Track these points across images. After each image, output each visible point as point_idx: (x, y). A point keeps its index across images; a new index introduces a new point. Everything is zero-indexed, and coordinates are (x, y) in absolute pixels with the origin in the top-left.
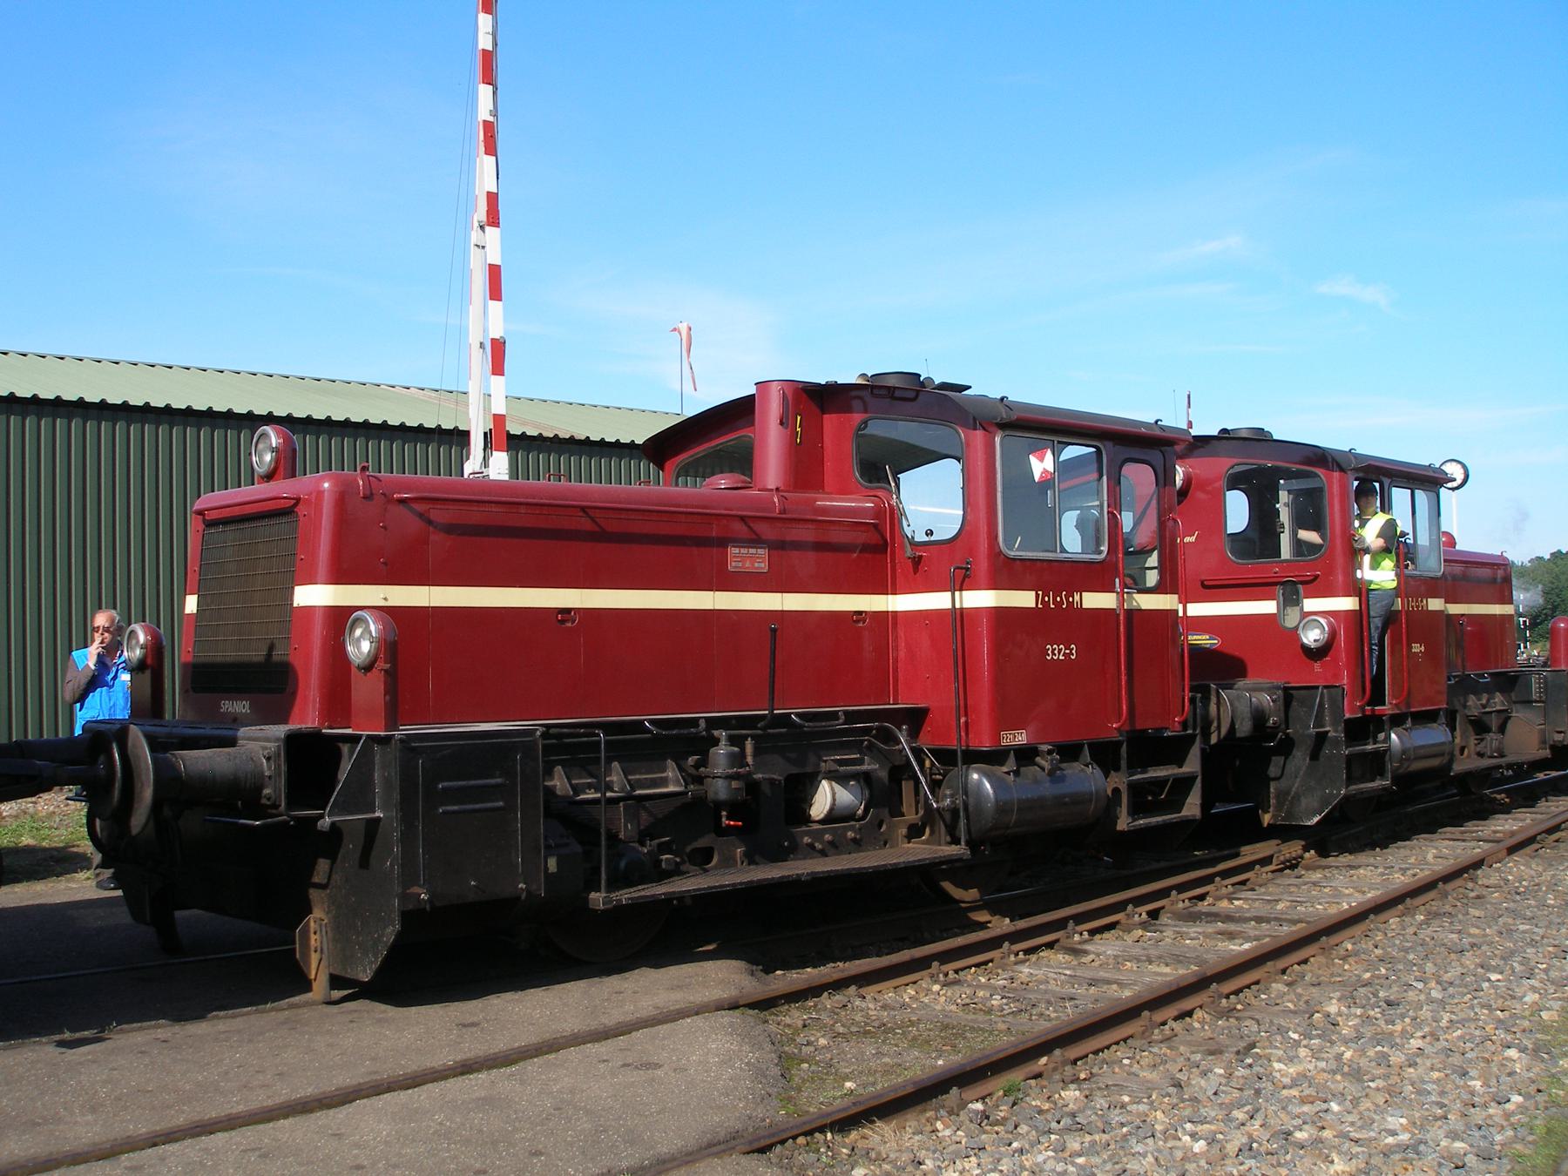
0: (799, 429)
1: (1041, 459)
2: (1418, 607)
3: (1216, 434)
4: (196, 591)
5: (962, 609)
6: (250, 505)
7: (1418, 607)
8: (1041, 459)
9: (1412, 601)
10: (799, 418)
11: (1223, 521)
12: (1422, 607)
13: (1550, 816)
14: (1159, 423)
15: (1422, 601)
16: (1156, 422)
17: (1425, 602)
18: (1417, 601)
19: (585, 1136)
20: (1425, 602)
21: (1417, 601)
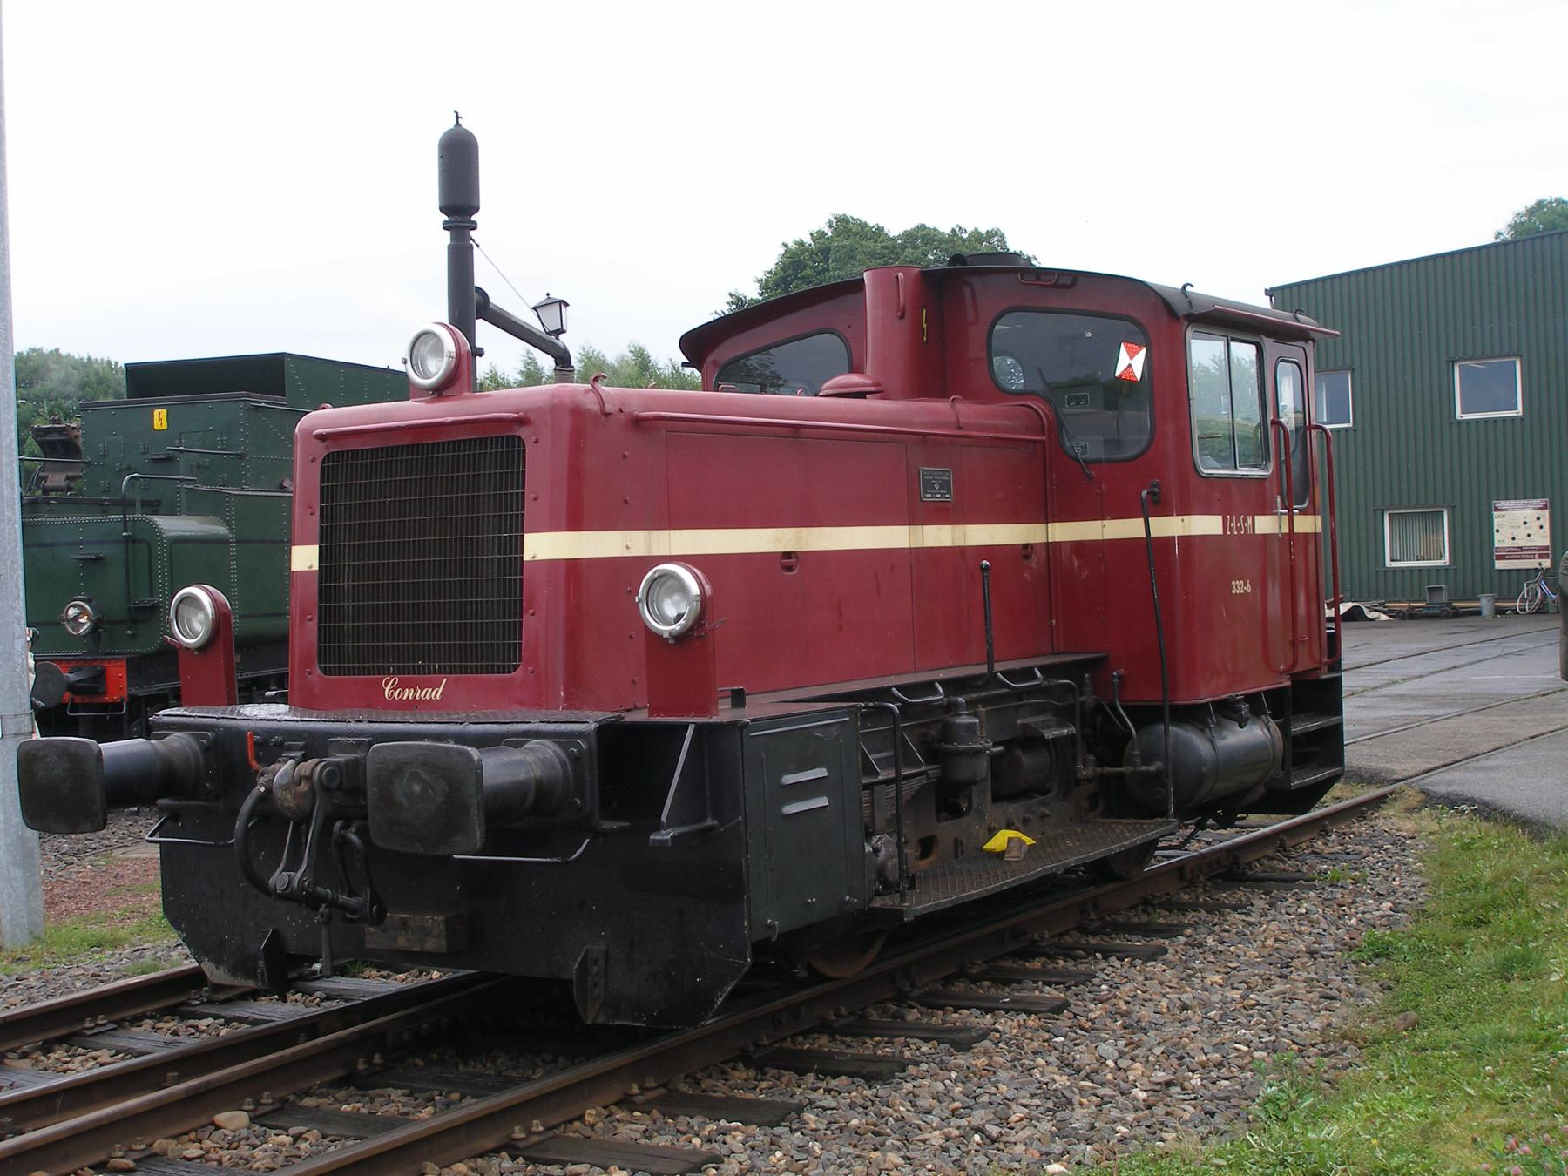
0: (925, 325)
1: (1132, 355)
2: (1239, 529)
3: (476, 284)
4: (318, 541)
5: (1314, 514)
6: (905, 436)
7: (1239, 529)
8: (1132, 355)
9: (1231, 521)
10: (925, 311)
11: (355, 445)
12: (1246, 528)
13: (1385, 691)
14: (1188, 288)
15: (1245, 520)
16: (1184, 287)
17: (1250, 521)
18: (1238, 520)
19: (61, 947)
20: (1250, 521)
21: (1238, 520)
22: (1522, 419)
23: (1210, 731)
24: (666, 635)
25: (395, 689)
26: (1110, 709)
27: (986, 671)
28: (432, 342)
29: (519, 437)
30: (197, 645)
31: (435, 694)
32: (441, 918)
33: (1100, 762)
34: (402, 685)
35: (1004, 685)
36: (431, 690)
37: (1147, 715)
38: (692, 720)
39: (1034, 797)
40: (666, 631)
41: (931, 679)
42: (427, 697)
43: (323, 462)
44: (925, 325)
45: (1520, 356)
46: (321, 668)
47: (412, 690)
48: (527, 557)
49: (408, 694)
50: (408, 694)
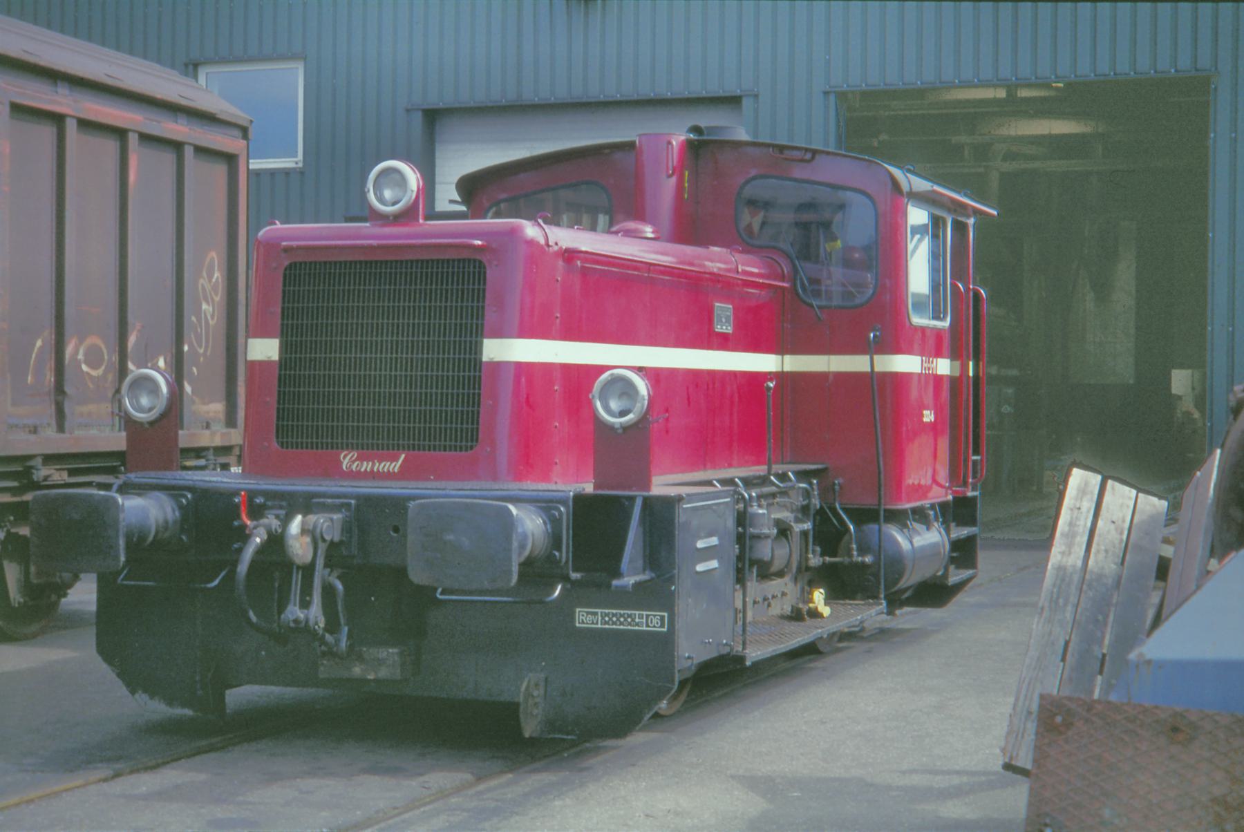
0: (686, 185)
10: (687, 174)
22: (301, 173)
23: (909, 531)
24: (617, 426)
25: (353, 462)
26: (830, 511)
27: (774, 466)
28: (396, 176)
29: (480, 262)
30: (149, 420)
31: (395, 466)
32: (396, 650)
33: (822, 555)
34: (361, 458)
35: (774, 484)
36: (389, 463)
37: (864, 516)
38: (639, 494)
39: (774, 580)
40: (617, 423)
41: (711, 478)
42: (386, 470)
43: (286, 269)
44: (686, 185)
45: (305, 59)
46: (278, 442)
47: (370, 463)
48: (485, 359)
49: (366, 466)
50: (366, 466)
